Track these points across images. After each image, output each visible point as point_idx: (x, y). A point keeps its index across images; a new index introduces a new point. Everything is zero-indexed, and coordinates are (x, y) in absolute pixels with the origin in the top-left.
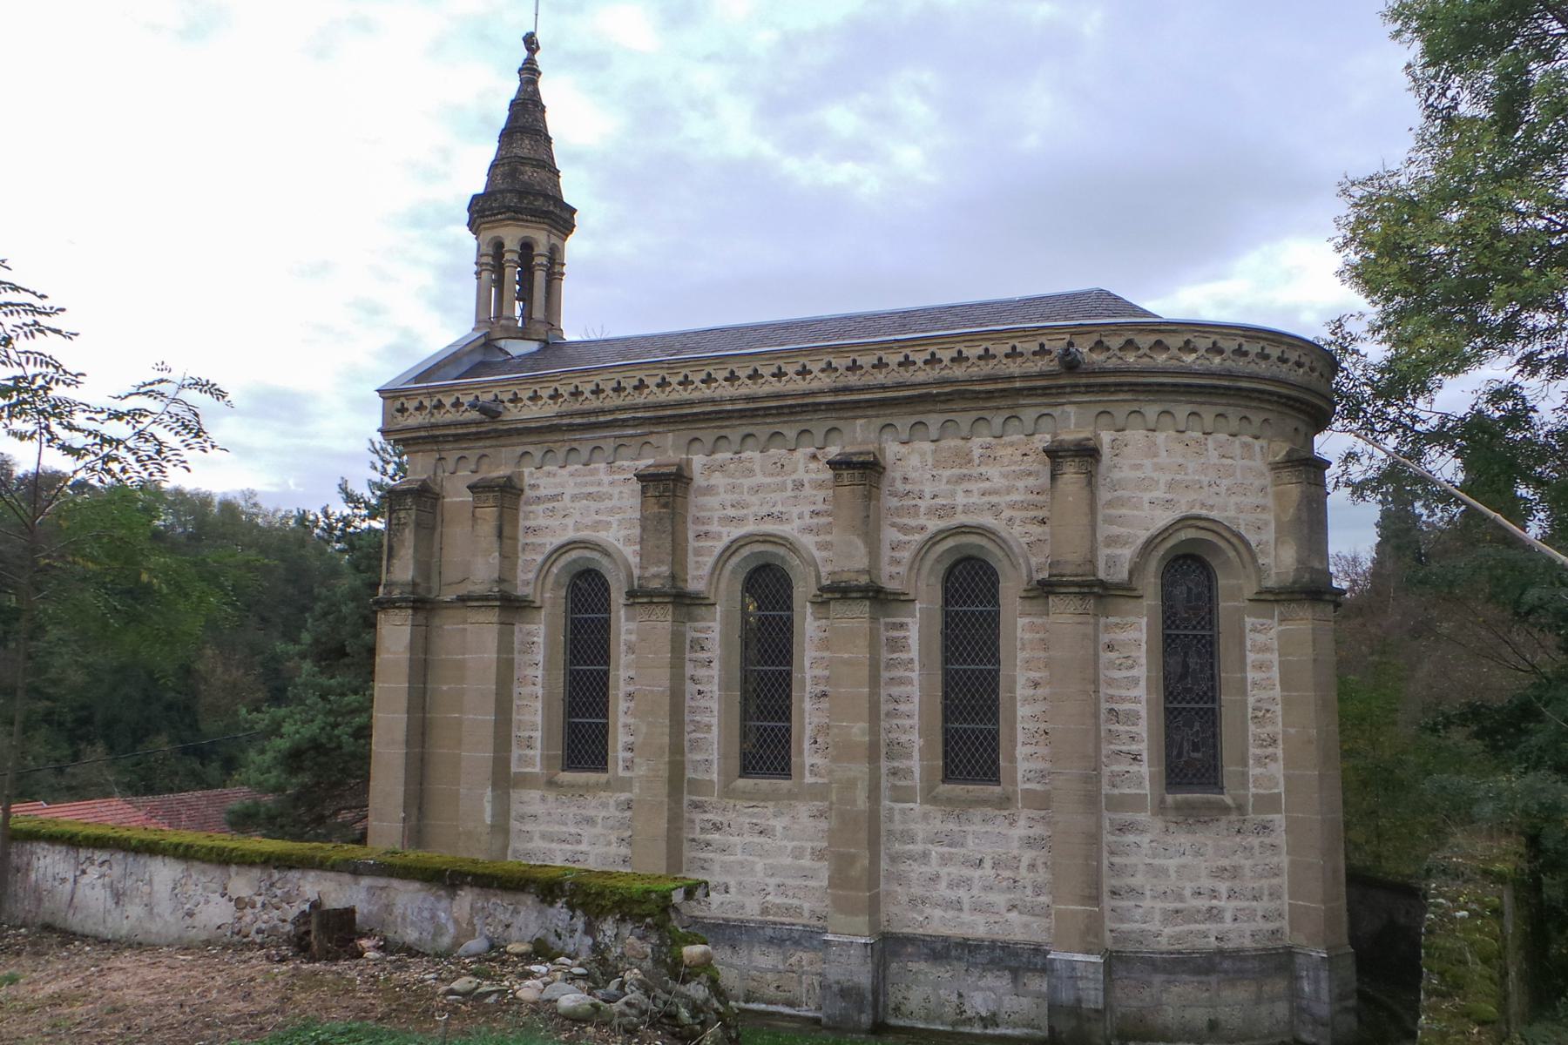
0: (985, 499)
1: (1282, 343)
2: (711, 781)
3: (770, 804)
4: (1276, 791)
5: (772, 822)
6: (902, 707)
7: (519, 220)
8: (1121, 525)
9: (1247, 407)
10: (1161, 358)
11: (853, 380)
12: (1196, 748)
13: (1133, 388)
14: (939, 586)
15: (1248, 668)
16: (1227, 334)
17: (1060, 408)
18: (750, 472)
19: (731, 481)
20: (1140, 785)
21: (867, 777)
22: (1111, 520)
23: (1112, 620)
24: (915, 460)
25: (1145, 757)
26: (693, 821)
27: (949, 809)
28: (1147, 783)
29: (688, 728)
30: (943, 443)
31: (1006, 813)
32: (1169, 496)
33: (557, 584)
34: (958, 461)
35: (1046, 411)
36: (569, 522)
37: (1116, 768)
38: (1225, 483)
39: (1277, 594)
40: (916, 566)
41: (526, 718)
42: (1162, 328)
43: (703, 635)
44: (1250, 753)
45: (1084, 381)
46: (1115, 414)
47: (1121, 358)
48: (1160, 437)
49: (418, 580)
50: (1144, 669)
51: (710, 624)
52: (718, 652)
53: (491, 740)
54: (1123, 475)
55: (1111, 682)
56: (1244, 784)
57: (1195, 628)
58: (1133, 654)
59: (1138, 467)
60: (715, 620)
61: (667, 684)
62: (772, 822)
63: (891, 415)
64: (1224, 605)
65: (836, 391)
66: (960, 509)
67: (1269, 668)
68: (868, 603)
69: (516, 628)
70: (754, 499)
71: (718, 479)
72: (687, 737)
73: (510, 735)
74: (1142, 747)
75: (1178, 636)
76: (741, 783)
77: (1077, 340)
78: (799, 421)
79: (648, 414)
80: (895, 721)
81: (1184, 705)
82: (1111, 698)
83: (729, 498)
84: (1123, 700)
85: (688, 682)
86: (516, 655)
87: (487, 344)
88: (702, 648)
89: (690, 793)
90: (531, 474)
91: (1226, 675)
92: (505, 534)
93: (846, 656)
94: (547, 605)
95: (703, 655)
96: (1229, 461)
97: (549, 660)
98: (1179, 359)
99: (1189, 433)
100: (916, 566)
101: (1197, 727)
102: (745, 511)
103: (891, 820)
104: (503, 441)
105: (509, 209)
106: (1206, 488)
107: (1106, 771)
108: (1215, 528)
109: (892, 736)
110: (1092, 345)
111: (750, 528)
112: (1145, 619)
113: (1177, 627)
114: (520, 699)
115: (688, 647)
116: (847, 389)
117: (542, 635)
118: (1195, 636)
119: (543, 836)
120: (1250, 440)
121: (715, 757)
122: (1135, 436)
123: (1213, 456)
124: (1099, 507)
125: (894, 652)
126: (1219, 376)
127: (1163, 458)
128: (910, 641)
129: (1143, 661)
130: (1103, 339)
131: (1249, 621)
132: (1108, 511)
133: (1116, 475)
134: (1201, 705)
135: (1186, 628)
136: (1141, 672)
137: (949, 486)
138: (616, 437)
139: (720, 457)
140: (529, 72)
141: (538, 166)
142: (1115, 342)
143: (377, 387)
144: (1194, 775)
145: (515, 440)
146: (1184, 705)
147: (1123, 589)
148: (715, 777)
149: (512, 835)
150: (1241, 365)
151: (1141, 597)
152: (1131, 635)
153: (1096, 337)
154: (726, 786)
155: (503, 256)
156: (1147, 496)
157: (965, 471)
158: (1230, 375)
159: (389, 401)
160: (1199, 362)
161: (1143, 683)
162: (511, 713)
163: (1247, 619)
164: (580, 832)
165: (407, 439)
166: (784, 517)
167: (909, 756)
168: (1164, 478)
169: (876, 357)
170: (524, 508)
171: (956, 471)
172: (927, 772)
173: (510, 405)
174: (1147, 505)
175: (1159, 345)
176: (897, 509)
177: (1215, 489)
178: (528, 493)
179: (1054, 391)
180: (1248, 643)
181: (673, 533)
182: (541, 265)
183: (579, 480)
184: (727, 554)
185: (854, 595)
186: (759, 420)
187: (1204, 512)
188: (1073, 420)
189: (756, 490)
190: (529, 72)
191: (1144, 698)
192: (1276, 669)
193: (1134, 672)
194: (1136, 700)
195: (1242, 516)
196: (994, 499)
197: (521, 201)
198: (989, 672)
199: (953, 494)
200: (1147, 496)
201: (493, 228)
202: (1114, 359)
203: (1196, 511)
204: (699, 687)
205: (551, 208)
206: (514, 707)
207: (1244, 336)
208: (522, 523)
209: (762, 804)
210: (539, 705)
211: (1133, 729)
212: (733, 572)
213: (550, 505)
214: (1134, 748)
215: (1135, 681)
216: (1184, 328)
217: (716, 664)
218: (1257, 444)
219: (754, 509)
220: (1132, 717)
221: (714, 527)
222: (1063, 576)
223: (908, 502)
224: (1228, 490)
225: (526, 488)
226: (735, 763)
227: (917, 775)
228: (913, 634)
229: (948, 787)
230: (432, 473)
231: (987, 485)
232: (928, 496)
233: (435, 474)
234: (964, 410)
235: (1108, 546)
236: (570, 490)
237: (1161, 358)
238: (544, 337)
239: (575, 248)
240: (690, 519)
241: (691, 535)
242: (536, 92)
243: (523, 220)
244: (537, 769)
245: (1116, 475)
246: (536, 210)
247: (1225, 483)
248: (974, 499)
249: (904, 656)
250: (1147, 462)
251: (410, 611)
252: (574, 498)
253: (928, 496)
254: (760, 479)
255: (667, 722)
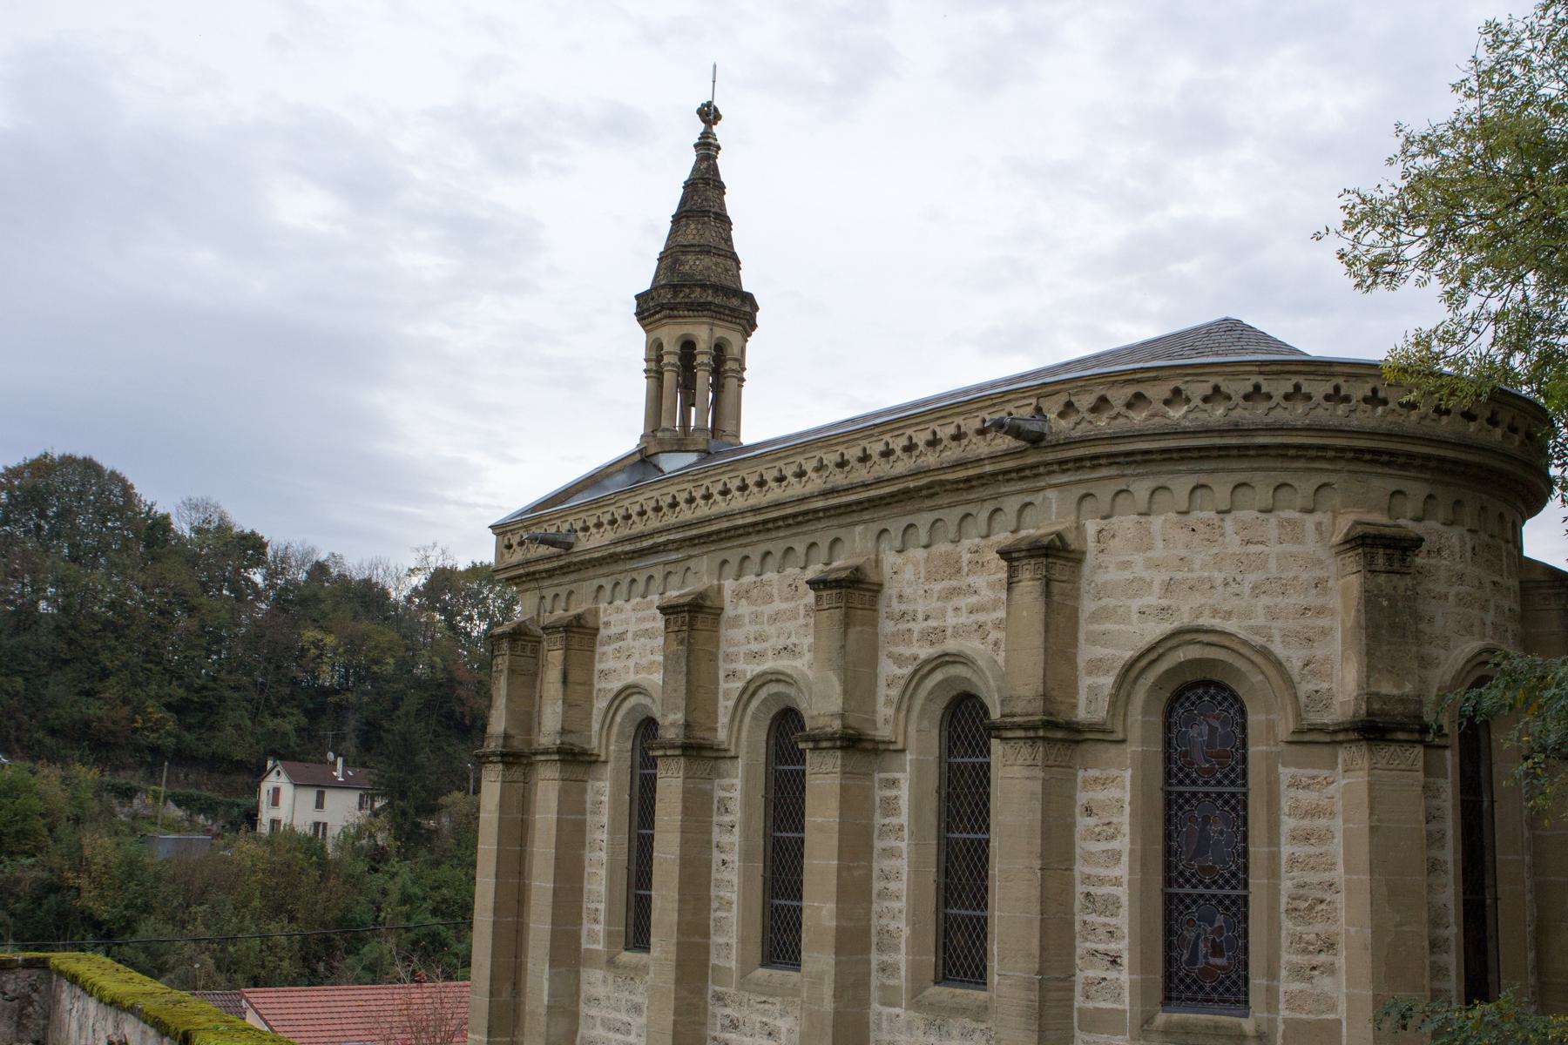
0: (973, 617)
1: (1333, 375)
2: (730, 969)
3: (778, 1000)
4: (1331, 1016)
5: (779, 1023)
6: (893, 886)
7: (675, 317)
8: (1105, 645)
9: (1286, 470)
10: (1138, 418)
11: (839, 479)
12: (1217, 950)
13: (1113, 459)
14: (936, 732)
15: (1283, 839)
16: (1232, 374)
17: (1041, 494)
18: (769, 599)
19: (754, 608)
20: (1118, 997)
21: (833, 972)
22: (1094, 639)
23: (1092, 773)
24: (908, 574)
25: (1125, 960)
26: (715, 1016)
27: (931, 1017)
28: (1126, 994)
29: (714, 905)
30: (933, 549)
31: (983, 1026)
32: (1164, 602)
33: (621, 734)
34: (949, 571)
35: (1028, 499)
36: (631, 663)
37: (1091, 973)
38: (1252, 578)
39: (1335, 732)
40: (904, 706)
41: (594, 887)
42: (1139, 376)
43: (728, 795)
44: (1283, 962)
45: (1050, 457)
46: (1171, 487)
47: (1090, 422)
48: (1156, 522)
49: (512, 732)
50: (1127, 839)
51: (897, 775)
52: (739, 815)
53: (549, 911)
54: (1108, 577)
55: (1089, 858)
56: (1272, 1005)
57: (1219, 783)
58: (1114, 820)
59: (1126, 565)
60: (737, 777)
61: (678, 852)
62: (779, 1023)
63: (884, 517)
64: (1255, 750)
65: (825, 494)
66: (949, 632)
67: (1325, 837)
68: (839, 753)
69: (589, 785)
70: (771, 630)
71: (744, 608)
72: (712, 916)
73: (581, 907)
74: (1121, 946)
75: (1194, 794)
76: (762, 973)
77: (1046, 404)
78: (805, 533)
79: (678, 536)
80: (887, 904)
81: (1201, 890)
82: (1087, 878)
83: (751, 629)
84: (1102, 881)
85: (715, 850)
86: (588, 817)
87: (642, 462)
88: (727, 810)
89: (714, 983)
90: (605, 610)
91: (1258, 850)
92: (571, 678)
93: (819, 820)
94: (612, 758)
95: (727, 819)
96: (1260, 548)
97: (614, 820)
98: (1164, 416)
99: (1196, 514)
100: (904, 706)
101: (1220, 920)
102: (765, 645)
103: (879, 1028)
104: (584, 574)
105: (662, 307)
106: (1221, 589)
107: (1080, 977)
108: (1227, 643)
109: (883, 921)
110: (1061, 409)
111: (769, 664)
112: (1129, 772)
113: (1194, 782)
114: (591, 865)
115: (715, 807)
116: (834, 491)
117: (607, 793)
118: (1220, 795)
119: (606, 1024)
120: (1296, 515)
121: (734, 941)
122: (1125, 523)
123: (1233, 543)
124: (1082, 621)
125: (888, 816)
126: (1222, 432)
127: (1159, 552)
128: (901, 802)
129: (1126, 829)
130: (1073, 399)
131: (1285, 773)
132: (1096, 627)
133: (1102, 577)
134: (1227, 891)
135: (1206, 783)
136: (1123, 844)
137: (940, 604)
138: (665, 564)
139: (748, 579)
140: (707, 148)
141: (701, 252)
142: (1157, 392)
143: (491, 523)
144: (1214, 989)
145: (591, 572)
146: (1201, 890)
147: (1099, 731)
148: (733, 964)
149: (581, 1021)
150: (1257, 413)
151: (1123, 741)
152: (1112, 793)
153: (1063, 398)
154: (743, 976)
155: (694, 357)
156: (1135, 604)
157: (954, 583)
158: (1236, 429)
159: (501, 537)
160: (1191, 416)
161: (1125, 859)
162: (582, 883)
163: (1281, 769)
164: (630, 1021)
165: (519, 577)
166: (797, 650)
167: (896, 949)
168: (1159, 578)
169: (860, 448)
170: (599, 650)
171: (947, 584)
172: (915, 968)
173: (580, 534)
174: (1135, 616)
175: (1138, 400)
176: (893, 635)
177: (1234, 588)
178: (603, 632)
179: (1252, 452)
180: (1285, 806)
181: (689, 673)
182: (702, 364)
183: (640, 614)
184: (745, 697)
185: (1401, 736)
186: (774, 534)
187: (1217, 623)
188: (1054, 507)
189: (774, 618)
190: (707, 148)
191: (1125, 880)
192: (1338, 840)
193: (1114, 845)
194: (1117, 882)
195: (1274, 624)
196: (981, 617)
197: (675, 295)
198: (980, 841)
199: (943, 613)
200: (1135, 604)
201: (657, 328)
202: (1083, 425)
203: (1206, 621)
204: (723, 856)
205: (709, 299)
206: (586, 874)
207: (1261, 373)
208: (598, 666)
209: (771, 1000)
210: (603, 872)
211: (1112, 921)
212: (754, 718)
213: (617, 645)
214: (1113, 947)
215: (1115, 856)
216: (1172, 372)
217: (736, 830)
218: (1310, 521)
219: (772, 642)
220: (1110, 906)
221: (740, 666)
222: (1014, 716)
223: (903, 626)
224: (1254, 588)
225: (602, 626)
226: (756, 952)
227: (903, 973)
228: (904, 793)
229: (938, 989)
230: (535, 613)
231: (974, 600)
232: (920, 616)
233: (539, 614)
234: (950, 506)
235: (1090, 673)
236: (632, 628)
237: (1138, 418)
238: (701, 447)
239: (758, 351)
240: (721, 656)
241: (722, 675)
242: (715, 170)
243: (680, 316)
244: (600, 947)
245: (1102, 577)
246: (692, 304)
247: (1252, 578)
248: (964, 619)
249: (894, 821)
250: (1138, 558)
251: (500, 766)
252: (636, 636)
253: (920, 616)
254: (778, 605)
255: (676, 896)
